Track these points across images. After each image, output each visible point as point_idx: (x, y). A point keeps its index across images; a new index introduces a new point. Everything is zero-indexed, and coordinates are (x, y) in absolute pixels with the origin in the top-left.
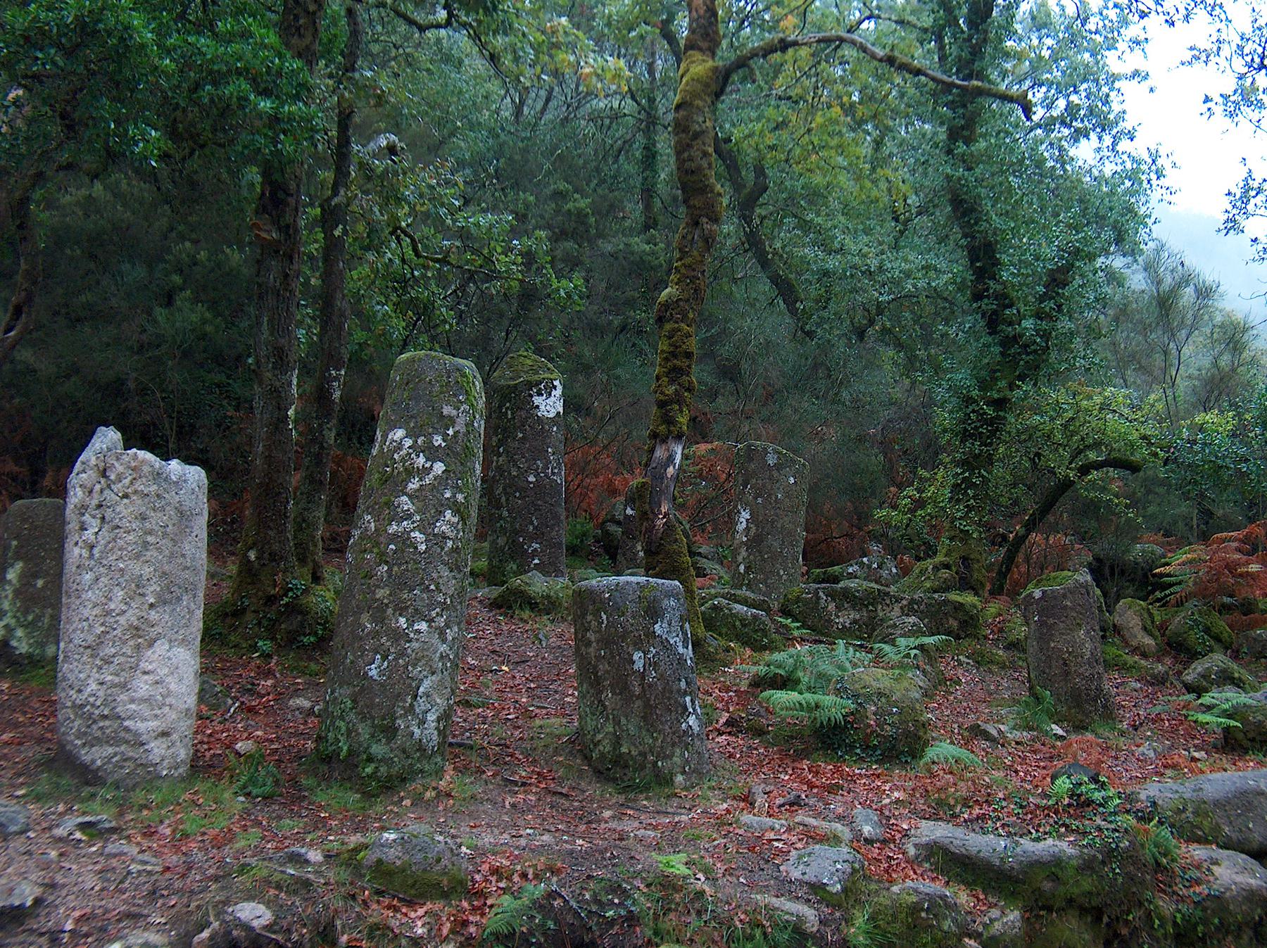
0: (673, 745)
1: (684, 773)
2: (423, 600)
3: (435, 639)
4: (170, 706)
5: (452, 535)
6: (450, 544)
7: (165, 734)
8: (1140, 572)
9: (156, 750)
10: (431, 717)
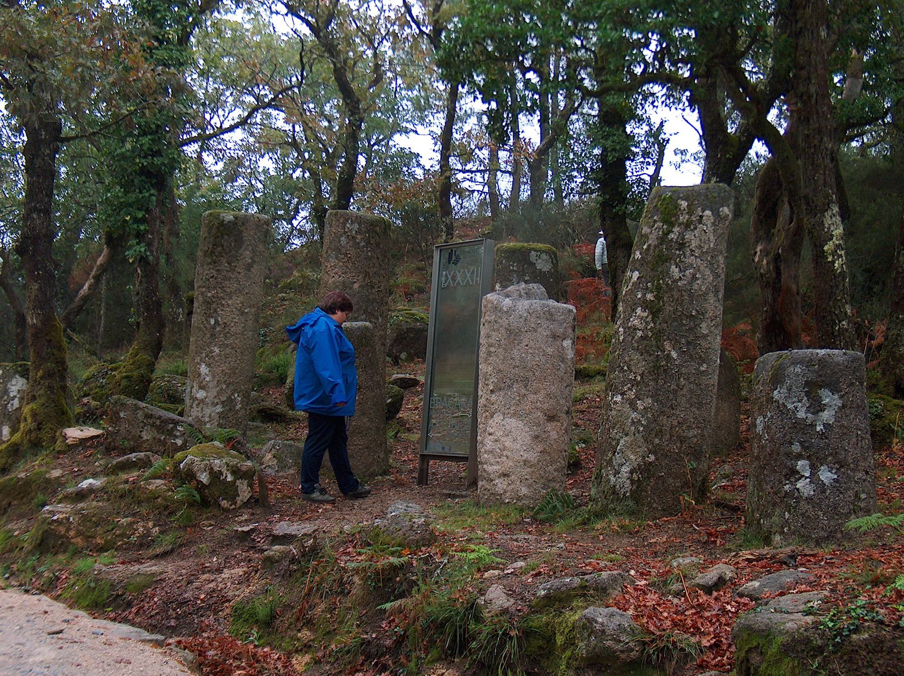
0: (774, 504)
1: (782, 533)
2: (619, 377)
3: (627, 408)
4: (507, 457)
5: (639, 326)
6: (640, 333)
7: (505, 475)
8: (291, 556)
9: (499, 485)
10: (625, 469)
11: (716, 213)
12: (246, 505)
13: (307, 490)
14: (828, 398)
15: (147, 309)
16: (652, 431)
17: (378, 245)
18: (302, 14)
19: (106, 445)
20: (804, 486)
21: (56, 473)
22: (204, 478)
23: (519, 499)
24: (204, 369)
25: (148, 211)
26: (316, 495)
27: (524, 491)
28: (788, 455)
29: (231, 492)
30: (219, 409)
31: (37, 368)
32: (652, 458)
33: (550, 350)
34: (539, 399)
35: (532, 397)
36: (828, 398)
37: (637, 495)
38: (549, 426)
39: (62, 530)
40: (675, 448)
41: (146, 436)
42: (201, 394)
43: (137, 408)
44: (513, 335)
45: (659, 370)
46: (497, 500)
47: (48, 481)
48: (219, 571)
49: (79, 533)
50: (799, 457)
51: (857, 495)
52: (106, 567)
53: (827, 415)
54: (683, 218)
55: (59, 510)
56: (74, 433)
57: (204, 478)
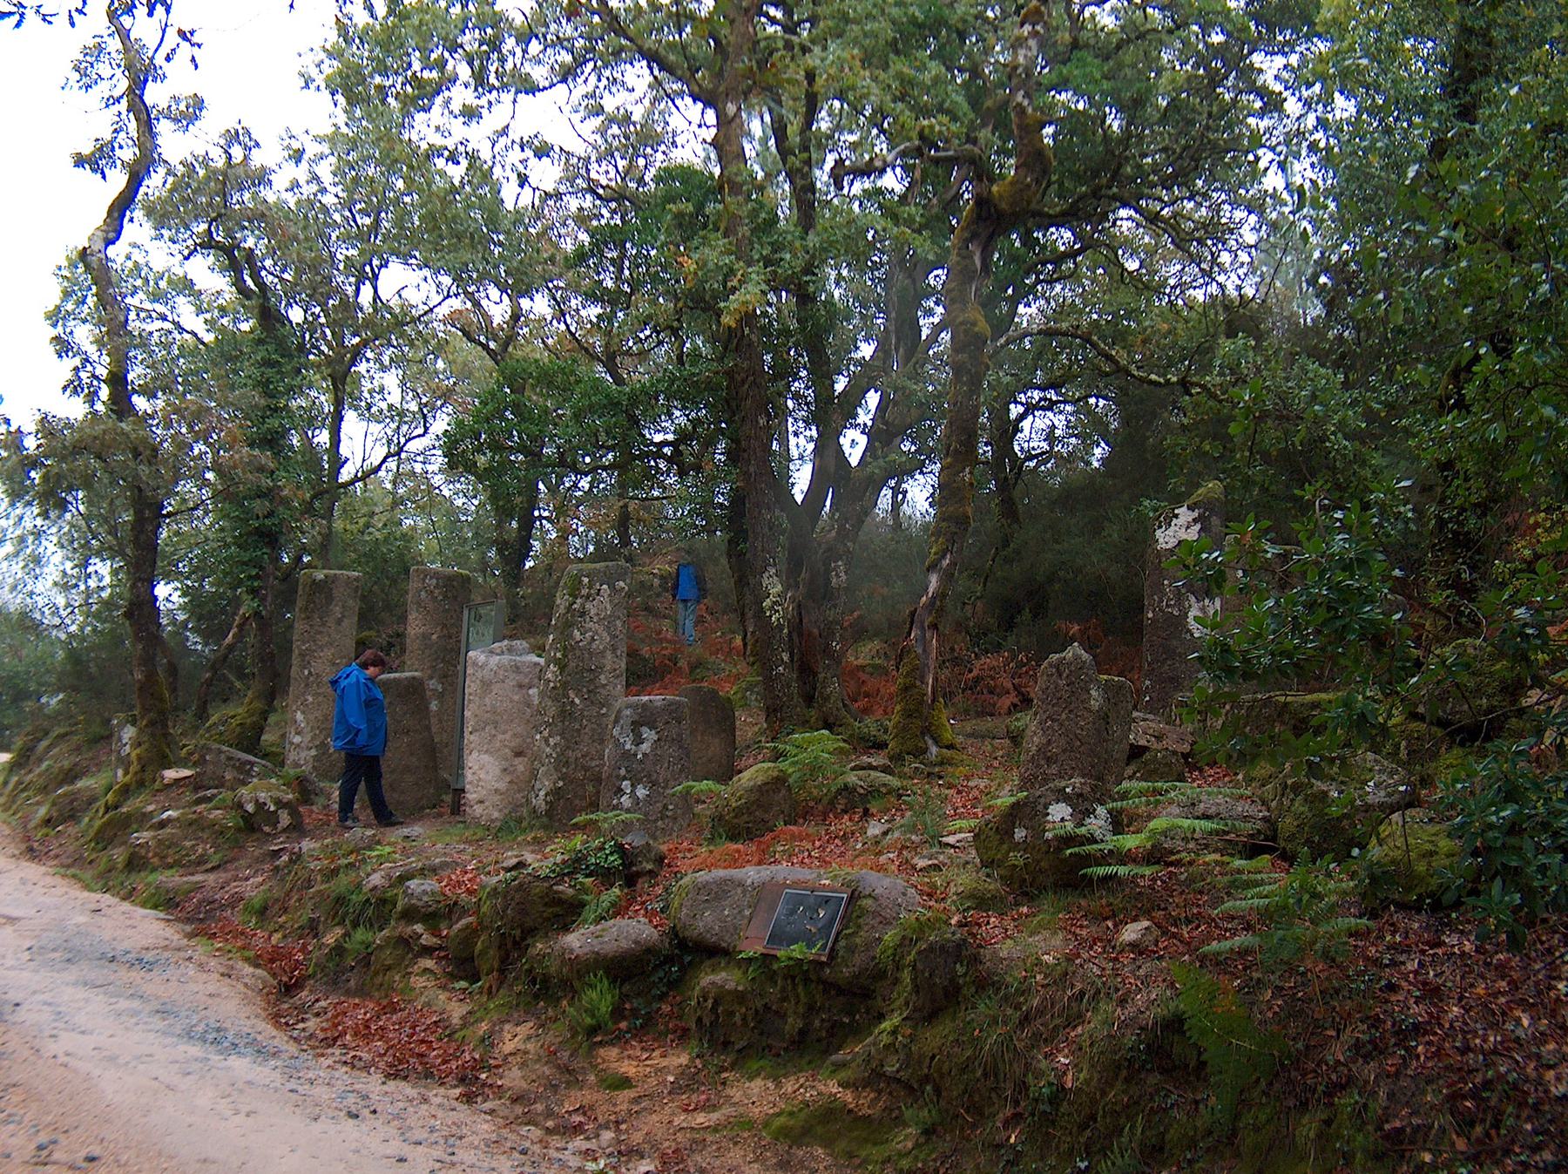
10: (542, 793)
11: (612, 587)
12: (284, 830)
13: (343, 819)
14: (649, 734)
15: (262, 660)
16: (561, 762)
17: (455, 598)
18: (482, 339)
19: (195, 784)
20: (625, 801)
21: (150, 808)
22: (250, 808)
23: (493, 821)
24: (299, 716)
25: (261, 568)
26: (349, 823)
27: (496, 815)
28: (618, 776)
29: (273, 819)
30: (313, 752)
31: (142, 718)
32: (561, 784)
33: (516, 698)
34: (506, 738)
35: (500, 737)
36: (649, 734)
37: (549, 813)
38: (517, 761)
39: (143, 852)
40: (580, 775)
41: (228, 777)
42: (297, 739)
43: (221, 752)
44: (486, 685)
45: (566, 714)
46: (476, 822)
47: (144, 814)
48: (247, 879)
49: (156, 855)
50: (625, 778)
51: (665, 807)
52: (171, 879)
53: (645, 747)
54: (584, 592)
55: (144, 836)
56: (170, 774)
57: (250, 808)
